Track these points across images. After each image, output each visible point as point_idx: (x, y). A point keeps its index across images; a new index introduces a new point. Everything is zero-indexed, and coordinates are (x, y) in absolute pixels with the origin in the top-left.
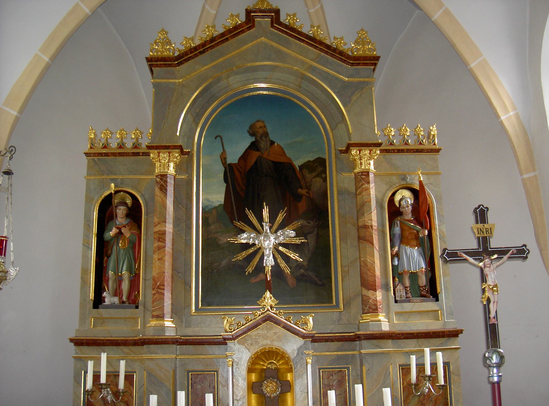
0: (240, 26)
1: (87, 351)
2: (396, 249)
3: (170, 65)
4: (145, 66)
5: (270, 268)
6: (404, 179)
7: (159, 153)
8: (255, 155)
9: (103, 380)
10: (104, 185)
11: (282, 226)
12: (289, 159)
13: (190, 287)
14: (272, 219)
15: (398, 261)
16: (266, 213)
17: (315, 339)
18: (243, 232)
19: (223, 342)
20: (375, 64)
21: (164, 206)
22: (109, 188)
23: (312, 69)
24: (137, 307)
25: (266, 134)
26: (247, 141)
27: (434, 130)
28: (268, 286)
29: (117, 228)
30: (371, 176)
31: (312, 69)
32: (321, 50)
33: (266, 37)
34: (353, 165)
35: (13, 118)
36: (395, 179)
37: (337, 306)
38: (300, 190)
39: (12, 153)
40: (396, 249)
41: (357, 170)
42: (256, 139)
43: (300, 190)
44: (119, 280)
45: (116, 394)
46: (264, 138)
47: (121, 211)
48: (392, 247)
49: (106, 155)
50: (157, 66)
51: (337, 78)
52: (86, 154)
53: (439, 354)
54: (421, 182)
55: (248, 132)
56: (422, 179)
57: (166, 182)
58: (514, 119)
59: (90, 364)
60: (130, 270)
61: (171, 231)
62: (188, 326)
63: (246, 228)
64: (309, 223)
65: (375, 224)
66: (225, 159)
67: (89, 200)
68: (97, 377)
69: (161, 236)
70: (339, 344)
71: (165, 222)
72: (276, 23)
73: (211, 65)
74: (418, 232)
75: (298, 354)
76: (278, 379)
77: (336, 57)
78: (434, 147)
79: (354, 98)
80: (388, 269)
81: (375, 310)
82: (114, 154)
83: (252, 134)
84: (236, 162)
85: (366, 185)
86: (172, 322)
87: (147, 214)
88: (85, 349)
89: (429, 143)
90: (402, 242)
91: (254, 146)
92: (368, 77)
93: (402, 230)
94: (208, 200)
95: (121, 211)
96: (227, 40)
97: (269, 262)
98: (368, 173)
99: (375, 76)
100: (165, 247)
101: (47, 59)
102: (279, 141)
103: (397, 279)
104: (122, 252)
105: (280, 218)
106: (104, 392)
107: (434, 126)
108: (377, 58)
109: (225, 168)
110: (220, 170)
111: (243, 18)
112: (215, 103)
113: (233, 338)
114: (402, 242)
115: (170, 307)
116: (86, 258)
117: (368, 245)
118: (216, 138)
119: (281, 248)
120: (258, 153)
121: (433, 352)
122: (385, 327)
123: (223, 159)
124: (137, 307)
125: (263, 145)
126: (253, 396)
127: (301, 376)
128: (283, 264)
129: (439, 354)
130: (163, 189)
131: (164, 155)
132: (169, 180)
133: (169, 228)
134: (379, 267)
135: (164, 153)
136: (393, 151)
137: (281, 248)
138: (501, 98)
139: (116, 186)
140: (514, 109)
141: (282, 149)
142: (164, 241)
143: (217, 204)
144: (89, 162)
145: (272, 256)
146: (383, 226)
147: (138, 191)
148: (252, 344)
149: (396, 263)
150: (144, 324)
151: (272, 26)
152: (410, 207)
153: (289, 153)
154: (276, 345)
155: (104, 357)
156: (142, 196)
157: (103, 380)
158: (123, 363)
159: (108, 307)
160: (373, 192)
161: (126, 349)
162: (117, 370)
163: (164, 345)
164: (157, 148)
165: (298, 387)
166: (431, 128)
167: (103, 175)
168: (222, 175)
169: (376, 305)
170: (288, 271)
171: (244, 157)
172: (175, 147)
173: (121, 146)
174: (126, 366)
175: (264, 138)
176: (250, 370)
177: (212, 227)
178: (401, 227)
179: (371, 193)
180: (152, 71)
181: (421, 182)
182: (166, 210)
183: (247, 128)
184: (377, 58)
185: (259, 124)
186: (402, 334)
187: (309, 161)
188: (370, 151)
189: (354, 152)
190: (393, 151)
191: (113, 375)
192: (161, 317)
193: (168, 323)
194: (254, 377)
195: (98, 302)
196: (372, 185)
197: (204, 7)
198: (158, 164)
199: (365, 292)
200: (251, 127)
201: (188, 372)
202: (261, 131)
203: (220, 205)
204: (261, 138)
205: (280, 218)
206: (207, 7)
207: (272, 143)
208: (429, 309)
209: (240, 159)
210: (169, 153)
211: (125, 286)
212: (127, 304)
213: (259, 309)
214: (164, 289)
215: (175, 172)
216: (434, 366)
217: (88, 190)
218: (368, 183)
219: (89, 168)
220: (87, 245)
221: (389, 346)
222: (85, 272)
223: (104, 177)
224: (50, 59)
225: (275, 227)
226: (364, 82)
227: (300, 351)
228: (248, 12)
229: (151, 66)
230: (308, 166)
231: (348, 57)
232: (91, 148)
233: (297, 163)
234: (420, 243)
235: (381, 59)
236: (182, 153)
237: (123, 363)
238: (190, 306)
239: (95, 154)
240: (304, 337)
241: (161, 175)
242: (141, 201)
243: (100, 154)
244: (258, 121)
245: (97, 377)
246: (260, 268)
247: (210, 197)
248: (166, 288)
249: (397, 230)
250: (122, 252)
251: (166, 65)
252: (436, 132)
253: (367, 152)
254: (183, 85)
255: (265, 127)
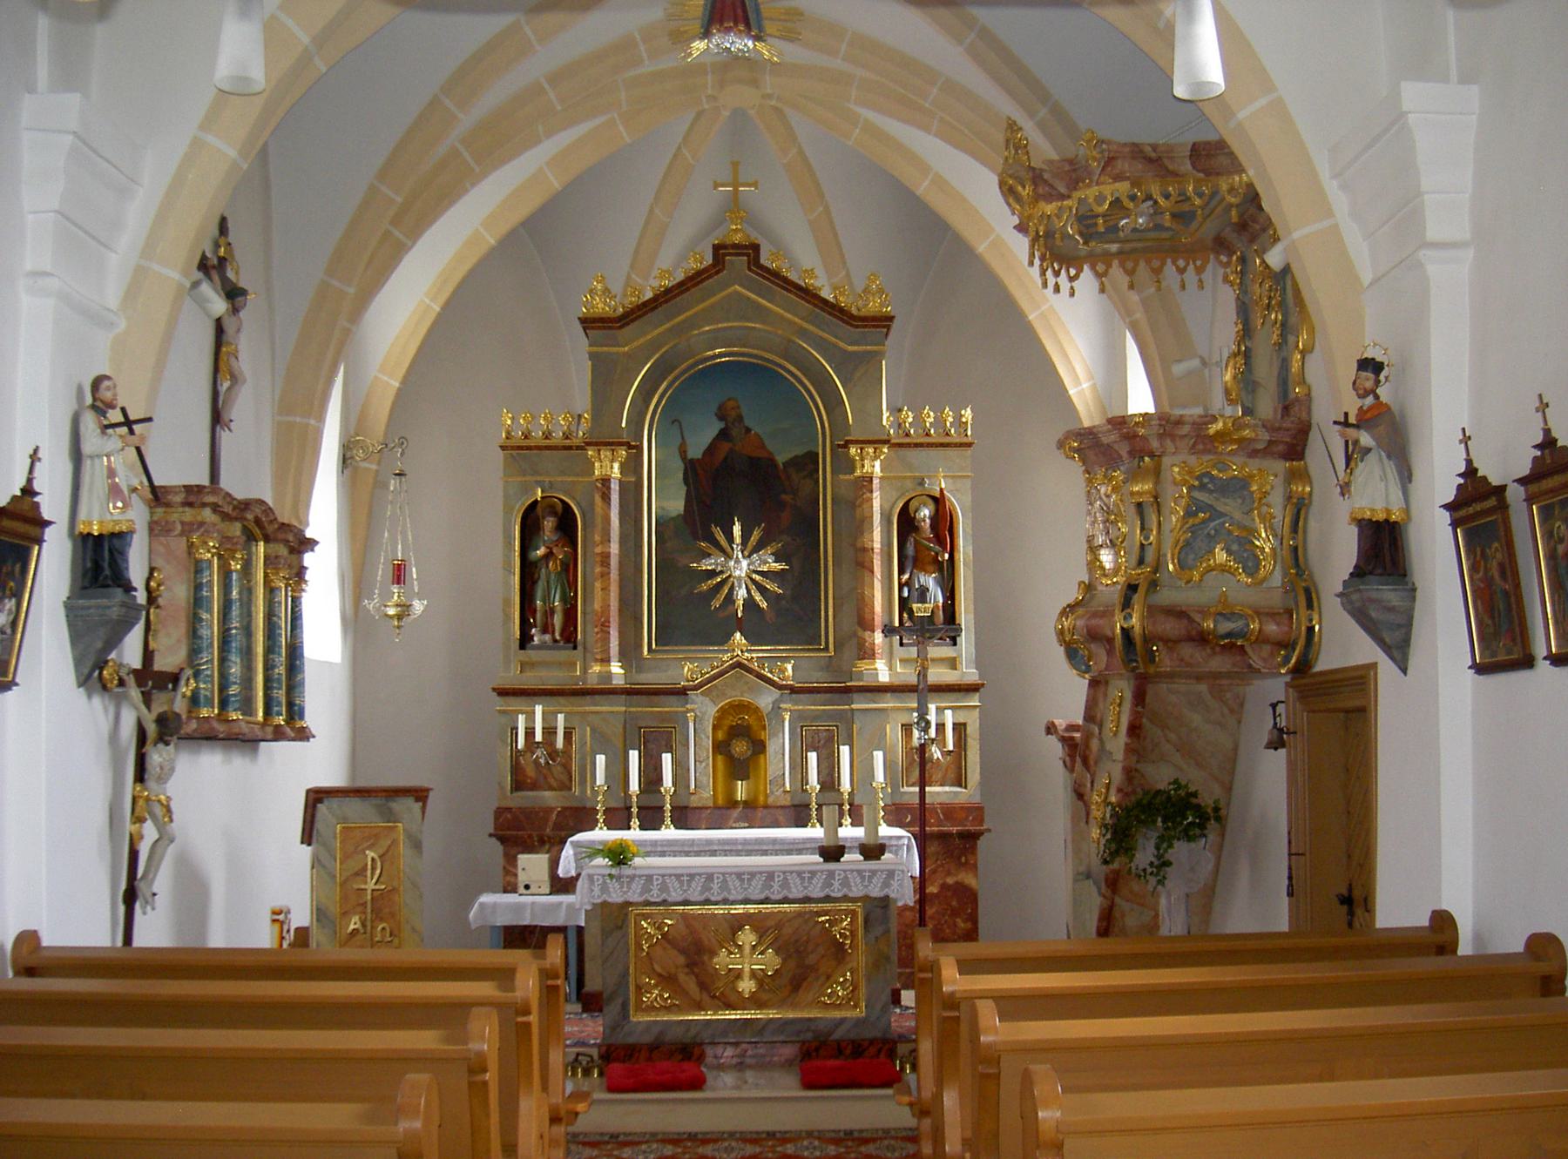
0: (706, 270)
1: (514, 704)
2: (906, 576)
3: (610, 328)
4: (579, 328)
5: (742, 602)
6: (922, 483)
7: (599, 450)
8: (725, 447)
9: (539, 737)
10: (527, 489)
11: (756, 549)
12: (770, 453)
13: (642, 623)
14: (745, 537)
15: (909, 592)
16: (737, 530)
17: (793, 690)
18: (709, 555)
19: (683, 692)
20: (889, 328)
21: (607, 520)
22: (536, 494)
23: (803, 334)
24: (575, 648)
25: (740, 418)
26: (717, 426)
27: (968, 414)
28: (740, 625)
29: (548, 548)
30: (876, 482)
31: (803, 334)
32: (815, 306)
33: (740, 285)
34: (850, 466)
35: (395, 389)
36: (909, 484)
37: (826, 649)
38: (784, 496)
39: (404, 446)
40: (906, 576)
41: (858, 473)
42: (726, 424)
43: (784, 496)
44: (551, 612)
45: (553, 754)
46: (736, 424)
47: (549, 524)
48: (901, 572)
49: (529, 448)
50: (593, 328)
51: (835, 346)
52: (503, 448)
53: (948, 713)
54: (941, 489)
55: (716, 414)
56: (943, 486)
57: (609, 488)
58: (1088, 393)
59: (521, 719)
60: (564, 599)
61: (617, 552)
62: (640, 670)
63: (713, 550)
64: (794, 540)
65: (877, 545)
66: (685, 452)
67: (508, 510)
68: (530, 733)
69: (605, 558)
70: (828, 695)
71: (609, 541)
72: (754, 265)
73: (667, 326)
74: (937, 554)
75: (773, 709)
76: (749, 736)
77: (835, 316)
78: (965, 440)
79: (858, 374)
80: (87, 954)
81: (871, 655)
82: (539, 448)
83: (721, 417)
84: (700, 457)
85: (869, 495)
86: (621, 667)
87: (584, 529)
88: (511, 699)
89: (959, 435)
90: (915, 566)
91: (723, 435)
92: (880, 345)
93: (917, 551)
94: (663, 509)
95: (549, 524)
96: (688, 289)
97: (741, 593)
98: (871, 479)
99: (886, 343)
100: (609, 573)
101: (438, 309)
102: (757, 429)
103: (905, 615)
104: (553, 576)
105: (756, 535)
106: (538, 752)
107: (969, 409)
108: (890, 319)
109: (685, 464)
110: (678, 467)
111: (709, 260)
112: (670, 378)
113: (696, 688)
114: (915, 566)
115: (617, 648)
116: (507, 585)
117: (867, 573)
118: (673, 422)
119: (754, 576)
120: (730, 445)
121: (940, 710)
122: (884, 677)
123: (683, 453)
124: (575, 648)
125: (734, 432)
126: (720, 757)
127: (775, 735)
128: (758, 597)
129: (948, 713)
130: (606, 498)
131: (606, 453)
132: (612, 486)
133: (614, 548)
134: (880, 601)
135: (605, 450)
136: (909, 445)
137: (754, 576)
138: (1070, 363)
139: (542, 492)
140: (1091, 377)
141: (761, 439)
142: (608, 565)
143: (674, 514)
144: (505, 459)
145: (744, 586)
146: (890, 545)
147: (573, 498)
148: (718, 696)
149: (906, 594)
150: (585, 670)
151: (750, 269)
152: (928, 521)
153: (770, 445)
154: (746, 698)
155: (539, 709)
156: (578, 505)
157: (539, 737)
158: (561, 717)
159: (539, 647)
160: (876, 504)
161: (562, 700)
162: (553, 725)
163: (611, 696)
164: (596, 444)
165: (771, 748)
166: (963, 412)
167: (524, 475)
168: (681, 475)
169: (874, 650)
170: (764, 605)
171: (710, 450)
172: (621, 444)
173: (547, 435)
174: (565, 720)
175: (736, 424)
176: (715, 728)
177: (669, 545)
178: (915, 547)
179: (874, 504)
180: (586, 334)
181: (941, 489)
182: (609, 525)
183: (714, 407)
184: (890, 319)
185: (731, 404)
186: (907, 686)
187: (796, 457)
188: (875, 449)
189: (853, 450)
190: (909, 445)
191: (550, 731)
192: (606, 661)
193: (616, 668)
194: (720, 735)
195: (525, 641)
196: (876, 494)
197: (651, 211)
198: (597, 465)
199: (860, 632)
200: (721, 407)
201: (641, 728)
202: (733, 413)
203: (679, 516)
204: (733, 424)
205: (756, 535)
206: (657, 211)
207: (748, 430)
208: (944, 656)
209: (705, 454)
210: (613, 450)
211: (558, 620)
212: (562, 644)
213: (727, 651)
214: (609, 627)
215: (621, 474)
216: (941, 727)
217: (506, 497)
218: (871, 492)
219: (506, 466)
220: (508, 568)
221: (888, 702)
222: (507, 602)
223: (528, 478)
224: (442, 309)
225: (746, 553)
226: (869, 352)
227: (776, 708)
228: (717, 248)
229: (585, 329)
230: (795, 463)
231: (852, 317)
232: (507, 438)
233: (781, 459)
234: (939, 566)
235: (895, 321)
236: (630, 447)
237: (561, 717)
238: (641, 646)
239: (513, 448)
240: (780, 687)
241: (602, 480)
242: (576, 512)
243: (520, 448)
244: (729, 400)
245: (530, 733)
246: (730, 600)
247: (665, 504)
248: (611, 625)
249: (910, 550)
250: (553, 576)
251: (604, 328)
252: (970, 417)
253: (871, 450)
254: (627, 355)
255: (738, 407)
